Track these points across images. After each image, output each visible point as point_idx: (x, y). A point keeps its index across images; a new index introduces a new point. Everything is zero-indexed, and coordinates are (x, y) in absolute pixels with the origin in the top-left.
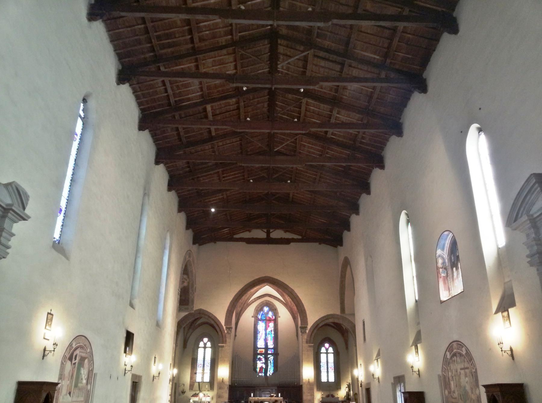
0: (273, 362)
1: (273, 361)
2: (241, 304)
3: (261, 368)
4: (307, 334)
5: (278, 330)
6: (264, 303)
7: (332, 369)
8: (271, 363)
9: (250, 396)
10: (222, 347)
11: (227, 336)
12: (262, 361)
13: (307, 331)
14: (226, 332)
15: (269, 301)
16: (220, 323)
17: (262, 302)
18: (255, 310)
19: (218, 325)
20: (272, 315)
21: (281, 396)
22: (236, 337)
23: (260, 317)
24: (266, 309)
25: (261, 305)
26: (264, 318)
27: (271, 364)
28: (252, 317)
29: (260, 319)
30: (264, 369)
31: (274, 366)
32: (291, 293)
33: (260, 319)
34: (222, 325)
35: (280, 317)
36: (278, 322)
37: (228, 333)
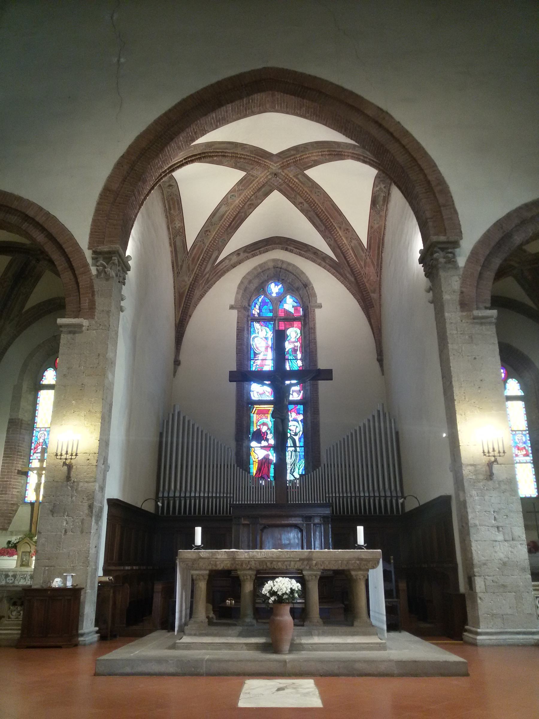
0: (302, 444)
1: (302, 440)
2: (193, 259)
3: (264, 463)
4: (461, 272)
5: (315, 343)
6: (269, 269)
7: (524, 452)
8: (295, 446)
9: (189, 543)
10: (75, 330)
11: (96, 288)
12: (267, 440)
13: (461, 261)
14: (93, 270)
15: (283, 262)
16: (71, 238)
17: (260, 266)
18: (239, 288)
19: (60, 247)
20: (295, 304)
21: (370, 543)
22: (180, 369)
23: (256, 311)
24: (275, 289)
25: (258, 276)
26: (271, 315)
27: (298, 449)
28: (232, 307)
29: (256, 316)
30: (272, 467)
31: (307, 456)
32: (376, 122)
33: (256, 316)
34: (77, 244)
35: (320, 306)
36: (314, 320)
37: (103, 275)
